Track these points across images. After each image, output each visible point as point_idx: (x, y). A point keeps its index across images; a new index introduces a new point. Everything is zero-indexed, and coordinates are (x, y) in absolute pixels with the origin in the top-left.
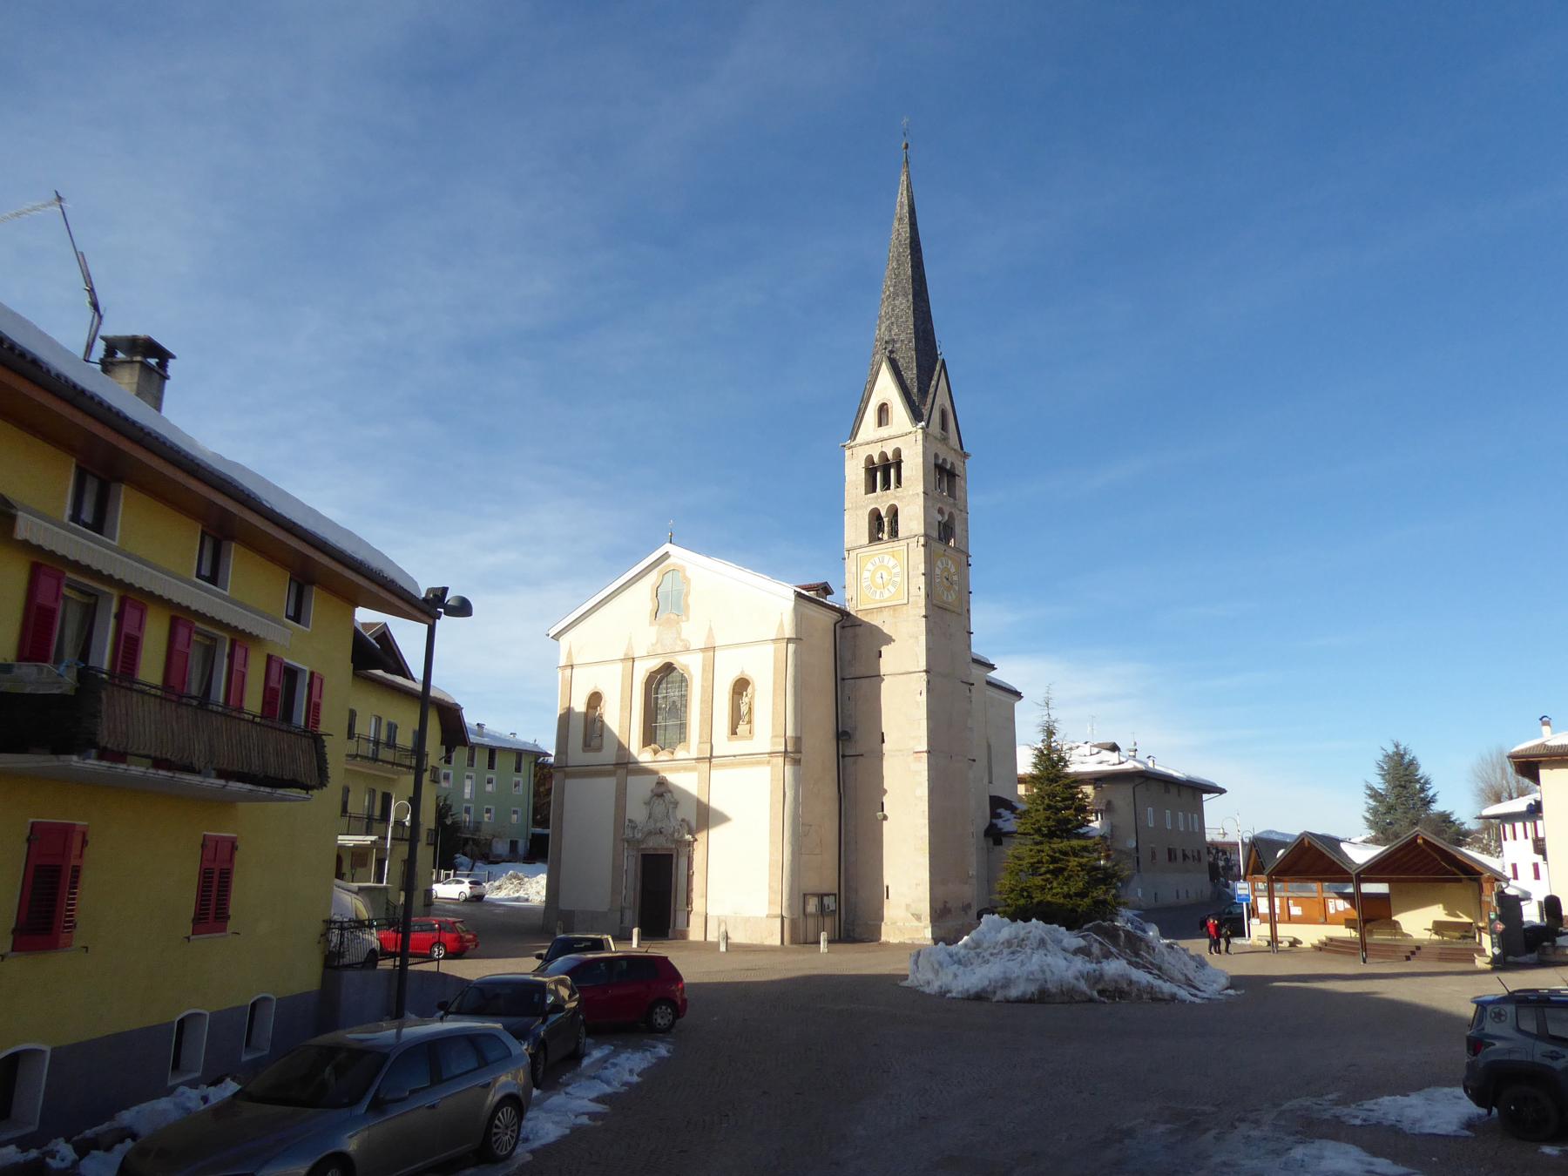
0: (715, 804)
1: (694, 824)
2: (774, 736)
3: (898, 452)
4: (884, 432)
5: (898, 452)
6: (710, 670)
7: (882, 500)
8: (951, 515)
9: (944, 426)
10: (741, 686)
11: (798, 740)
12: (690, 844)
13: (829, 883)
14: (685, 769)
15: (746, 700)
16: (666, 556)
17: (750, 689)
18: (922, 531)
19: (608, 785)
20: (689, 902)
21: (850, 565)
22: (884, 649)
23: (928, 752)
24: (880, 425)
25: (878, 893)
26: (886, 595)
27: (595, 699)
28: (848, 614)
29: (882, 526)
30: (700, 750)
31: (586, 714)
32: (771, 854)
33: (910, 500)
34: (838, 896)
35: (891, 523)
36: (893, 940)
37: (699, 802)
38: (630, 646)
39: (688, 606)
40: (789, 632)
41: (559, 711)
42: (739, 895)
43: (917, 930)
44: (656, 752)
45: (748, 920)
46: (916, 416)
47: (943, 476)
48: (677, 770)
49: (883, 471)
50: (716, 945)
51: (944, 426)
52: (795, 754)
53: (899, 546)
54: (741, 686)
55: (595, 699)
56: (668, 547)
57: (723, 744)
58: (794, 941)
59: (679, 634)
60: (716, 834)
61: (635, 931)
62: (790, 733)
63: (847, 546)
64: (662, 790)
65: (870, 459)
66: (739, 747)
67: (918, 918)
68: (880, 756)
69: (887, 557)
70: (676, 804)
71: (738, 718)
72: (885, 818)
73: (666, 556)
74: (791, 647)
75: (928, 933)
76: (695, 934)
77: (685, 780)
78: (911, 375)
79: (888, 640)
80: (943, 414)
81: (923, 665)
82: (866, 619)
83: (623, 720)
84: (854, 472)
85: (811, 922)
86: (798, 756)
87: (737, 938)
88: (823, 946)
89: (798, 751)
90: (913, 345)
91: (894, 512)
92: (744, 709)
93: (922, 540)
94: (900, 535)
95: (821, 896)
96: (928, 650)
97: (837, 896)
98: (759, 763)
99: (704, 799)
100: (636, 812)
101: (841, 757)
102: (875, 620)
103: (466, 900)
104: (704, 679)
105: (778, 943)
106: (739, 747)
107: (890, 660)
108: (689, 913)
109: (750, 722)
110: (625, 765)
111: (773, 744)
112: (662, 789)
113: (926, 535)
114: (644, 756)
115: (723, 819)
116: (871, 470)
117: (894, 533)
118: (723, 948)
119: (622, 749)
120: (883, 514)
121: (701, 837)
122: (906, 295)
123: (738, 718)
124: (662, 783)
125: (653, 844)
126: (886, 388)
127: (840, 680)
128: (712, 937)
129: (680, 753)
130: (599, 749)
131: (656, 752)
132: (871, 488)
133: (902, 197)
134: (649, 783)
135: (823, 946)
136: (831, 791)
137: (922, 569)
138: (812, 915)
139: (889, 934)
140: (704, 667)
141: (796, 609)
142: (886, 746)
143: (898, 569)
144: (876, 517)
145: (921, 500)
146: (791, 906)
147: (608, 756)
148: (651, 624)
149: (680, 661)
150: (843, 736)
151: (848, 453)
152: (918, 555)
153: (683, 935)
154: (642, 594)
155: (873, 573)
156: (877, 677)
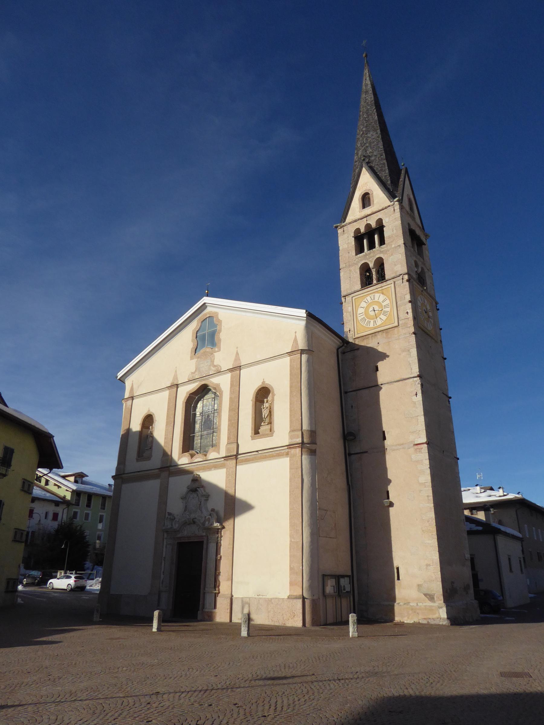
0: (240, 494)
1: (222, 514)
2: (292, 431)
3: (380, 221)
4: (368, 211)
5: (380, 221)
6: (236, 385)
7: (369, 257)
8: (422, 269)
9: (411, 209)
10: (263, 394)
11: (313, 433)
12: (218, 531)
13: (344, 568)
14: (216, 467)
15: (266, 405)
16: (204, 306)
17: (270, 398)
18: (406, 271)
19: (154, 485)
20: (216, 584)
21: (347, 307)
22: (380, 364)
23: (428, 443)
24: (364, 207)
25: (388, 576)
26: (379, 322)
27: (148, 420)
30: (228, 450)
31: (141, 433)
32: (291, 536)
33: (394, 255)
35: (377, 272)
36: (407, 620)
37: (226, 494)
38: (176, 377)
39: (220, 340)
40: (302, 344)
41: (122, 433)
42: (263, 568)
44: (192, 456)
45: (269, 601)
46: (391, 194)
47: (414, 240)
48: (209, 468)
50: (238, 627)
51: (411, 209)
52: (310, 444)
53: (388, 286)
54: (263, 394)
55: (148, 420)
56: (206, 300)
57: (247, 443)
58: (315, 623)
59: (213, 361)
60: (242, 522)
61: (156, 613)
62: (305, 427)
63: (343, 294)
64: (197, 486)
65: (358, 230)
66: (262, 443)
67: (431, 597)
68: (382, 451)
69: (377, 295)
70: (207, 497)
71: (261, 421)
72: (391, 504)
73: (204, 306)
74: (304, 357)
75: (443, 613)
76: (221, 616)
77: (215, 477)
78: (385, 174)
79: (383, 356)
80: (410, 200)
81: (416, 371)
82: (362, 344)
83: (167, 435)
85: (330, 602)
86: (313, 447)
87: (259, 619)
88: (352, 630)
89: (313, 441)
91: (380, 264)
92: (265, 413)
93: (406, 277)
94: (387, 277)
95: (338, 578)
96: (420, 360)
97: (350, 580)
98: (279, 456)
99: (231, 491)
100: (175, 506)
101: (348, 455)
102: (371, 343)
103: (72, 590)
104: (232, 392)
105: (299, 624)
106: (262, 443)
107: (385, 372)
108: (216, 595)
109: (270, 423)
110: (168, 468)
111: (291, 437)
112: (196, 485)
113: (408, 274)
114: (182, 460)
115: (247, 507)
116: (359, 238)
117: (382, 278)
118: (244, 633)
119: (166, 456)
120: (371, 265)
121: (228, 524)
122: (375, 130)
123: (261, 421)
124: (197, 480)
125: (188, 532)
126: (366, 182)
127: (344, 392)
128: (237, 618)
129: (212, 455)
130: (149, 458)
131: (192, 456)
132: (360, 249)
133: (367, 97)
134: (186, 480)
135: (352, 630)
136: (340, 482)
137: (408, 297)
139: (403, 615)
140: (232, 382)
141: (307, 327)
142: (387, 443)
143: (388, 302)
144: (365, 269)
145: (402, 250)
146: (311, 587)
147: (155, 462)
148: (192, 358)
149: (214, 381)
150: (349, 437)
152: (404, 290)
153: (210, 617)
154: (186, 339)
156: (376, 387)
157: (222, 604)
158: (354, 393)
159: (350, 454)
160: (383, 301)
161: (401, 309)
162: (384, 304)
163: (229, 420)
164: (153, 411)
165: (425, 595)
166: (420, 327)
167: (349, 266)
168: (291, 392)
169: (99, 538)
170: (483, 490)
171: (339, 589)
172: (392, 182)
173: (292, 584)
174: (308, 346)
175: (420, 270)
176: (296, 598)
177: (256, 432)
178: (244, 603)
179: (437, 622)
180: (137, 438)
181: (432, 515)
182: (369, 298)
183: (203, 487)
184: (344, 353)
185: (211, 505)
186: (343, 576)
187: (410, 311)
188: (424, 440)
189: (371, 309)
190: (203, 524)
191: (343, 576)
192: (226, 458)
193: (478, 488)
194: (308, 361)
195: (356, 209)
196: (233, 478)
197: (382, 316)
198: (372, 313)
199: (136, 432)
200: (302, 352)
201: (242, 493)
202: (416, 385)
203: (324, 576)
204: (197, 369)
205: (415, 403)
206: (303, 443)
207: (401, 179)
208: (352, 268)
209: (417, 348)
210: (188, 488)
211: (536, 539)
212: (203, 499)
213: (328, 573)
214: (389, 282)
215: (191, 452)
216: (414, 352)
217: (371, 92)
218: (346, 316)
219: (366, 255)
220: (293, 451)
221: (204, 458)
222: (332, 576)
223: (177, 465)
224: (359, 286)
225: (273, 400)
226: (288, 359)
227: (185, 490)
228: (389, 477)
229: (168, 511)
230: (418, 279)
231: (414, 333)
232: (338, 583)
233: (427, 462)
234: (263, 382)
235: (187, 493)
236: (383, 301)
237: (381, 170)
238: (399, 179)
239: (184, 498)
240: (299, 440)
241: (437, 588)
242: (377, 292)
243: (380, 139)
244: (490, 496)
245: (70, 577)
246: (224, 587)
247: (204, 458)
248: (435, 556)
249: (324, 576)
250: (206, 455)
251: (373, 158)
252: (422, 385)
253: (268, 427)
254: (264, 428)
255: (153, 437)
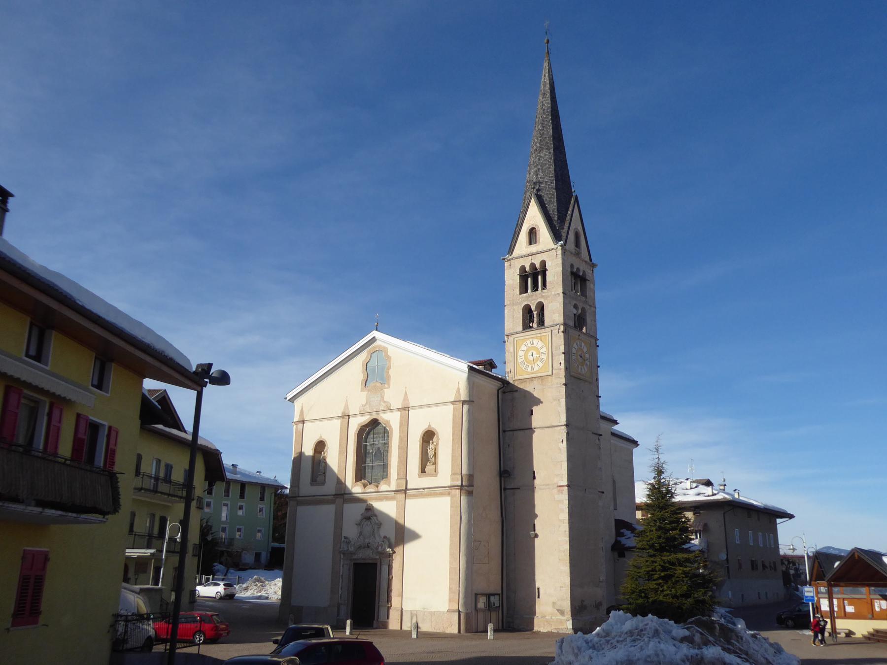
0: (409, 524)
1: (393, 540)
2: (453, 474)
3: (543, 263)
4: (533, 248)
5: (543, 263)
6: (405, 424)
7: (532, 299)
9: (577, 244)
10: (429, 436)
11: (471, 477)
12: (390, 556)
13: (494, 585)
15: (432, 446)
16: (374, 340)
17: (435, 439)
18: (562, 321)
19: (330, 509)
20: (389, 599)
21: (509, 347)
22: (535, 409)
23: (569, 486)
24: (530, 243)
25: (532, 594)
26: (536, 368)
27: (320, 446)
28: (508, 383)
29: (533, 318)
30: (398, 484)
31: (313, 457)
32: (451, 563)
33: (553, 299)
34: (501, 596)
36: (543, 630)
37: (397, 523)
38: (346, 407)
40: (464, 396)
42: (427, 588)
43: (561, 622)
44: (365, 486)
45: (433, 613)
46: (557, 236)
48: (380, 499)
49: (533, 277)
51: (577, 244)
53: (545, 333)
54: (429, 436)
55: (320, 446)
56: (375, 334)
57: (415, 481)
58: (468, 630)
59: (383, 397)
60: (410, 549)
61: (348, 622)
63: (507, 332)
64: (370, 514)
65: (523, 268)
66: (427, 482)
67: (562, 612)
68: (532, 489)
69: (536, 341)
70: (380, 525)
71: (427, 461)
72: (536, 536)
73: (374, 340)
74: (466, 407)
75: (569, 625)
77: (387, 507)
78: (552, 207)
79: (538, 402)
81: (563, 420)
82: (521, 386)
83: (341, 461)
84: (512, 278)
85: (481, 616)
86: (470, 489)
87: (425, 627)
88: (490, 634)
89: (471, 485)
90: (554, 185)
91: (541, 307)
92: (431, 453)
93: (562, 328)
94: (546, 324)
95: (489, 596)
97: (498, 596)
98: (442, 494)
99: (401, 521)
100: (350, 531)
101: (503, 489)
102: (528, 387)
103: (222, 598)
104: (401, 431)
105: (456, 631)
106: (427, 482)
107: (539, 416)
108: (389, 608)
109: (435, 463)
110: (342, 495)
111: (452, 480)
113: (565, 324)
114: (357, 489)
115: (415, 536)
116: (523, 276)
117: (541, 323)
118: (414, 636)
119: (340, 484)
120: (533, 308)
121: (398, 550)
122: (548, 149)
123: (427, 461)
124: (370, 509)
125: (364, 555)
126: (534, 216)
128: (406, 627)
129: (383, 487)
131: (365, 486)
132: (524, 289)
134: (360, 509)
135: (490, 634)
136: (495, 514)
137: (562, 349)
138: (481, 610)
139: (540, 625)
141: (469, 379)
142: (537, 482)
144: (527, 311)
146: (466, 604)
147: (329, 488)
148: (362, 390)
149: (384, 417)
151: (507, 264)
153: (385, 625)
155: (526, 352)
156: (530, 430)
157: (394, 616)
158: (511, 433)
159: (505, 489)
160: (541, 348)
161: (555, 358)
162: (541, 351)
163: (399, 457)
164: (325, 438)
165: (558, 610)
166: (571, 376)
167: (513, 304)
168: (453, 440)
169: (224, 530)
170: (694, 485)
171: (489, 605)
172: (559, 218)
173: (450, 601)
174: (470, 396)
175: (580, 311)
176: (454, 611)
177: (423, 471)
178: (413, 614)
179: (564, 631)
180: (310, 463)
181: (567, 547)
182: (528, 342)
183: (376, 516)
184: (504, 392)
185: (383, 533)
186: (493, 595)
187: (563, 362)
188: (566, 483)
189: (530, 354)
190: (377, 549)
191: (493, 595)
192: (396, 491)
193: (688, 482)
194: (469, 410)
195: (522, 245)
196: (402, 509)
197: (539, 363)
198: (531, 358)
199: (309, 456)
200: (464, 402)
201: (410, 523)
202: (562, 433)
203: (476, 594)
204: (368, 402)
205: (560, 449)
206: (462, 485)
207: (571, 205)
208: (516, 307)
209: (567, 397)
210: (362, 515)
211: (752, 544)
212: (376, 527)
213: (479, 592)
214: (547, 330)
215: (363, 481)
216: (563, 402)
217: (548, 95)
218: (508, 357)
219: (529, 296)
220: (453, 492)
221: (376, 489)
222: (482, 594)
223: (351, 493)
224: (520, 328)
225: (437, 445)
226: (451, 407)
227: (359, 517)
228: (536, 512)
229: (343, 535)
230: (578, 322)
231: (565, 385)
232: (489, 601)
233: (566, 502)
234: (429, 426)
235: (362, 520)
236: (541, 348)
237: (550, 202)
238: (567, 210)
239: (359, 524)
240: (459, 483)
241: (567, 605)
242: (536, 338)
243: (552, 161)
244: (699, 494)
245: (218, 585)
246: (395, 601)
247: (376, 489)
248: (567, 580)
249: (476, 594)
250: (377, 487)
251: (543, 185)
252: (568, 434)
253: (433, 467)
254: (430, 468)
255: (326, 463)
